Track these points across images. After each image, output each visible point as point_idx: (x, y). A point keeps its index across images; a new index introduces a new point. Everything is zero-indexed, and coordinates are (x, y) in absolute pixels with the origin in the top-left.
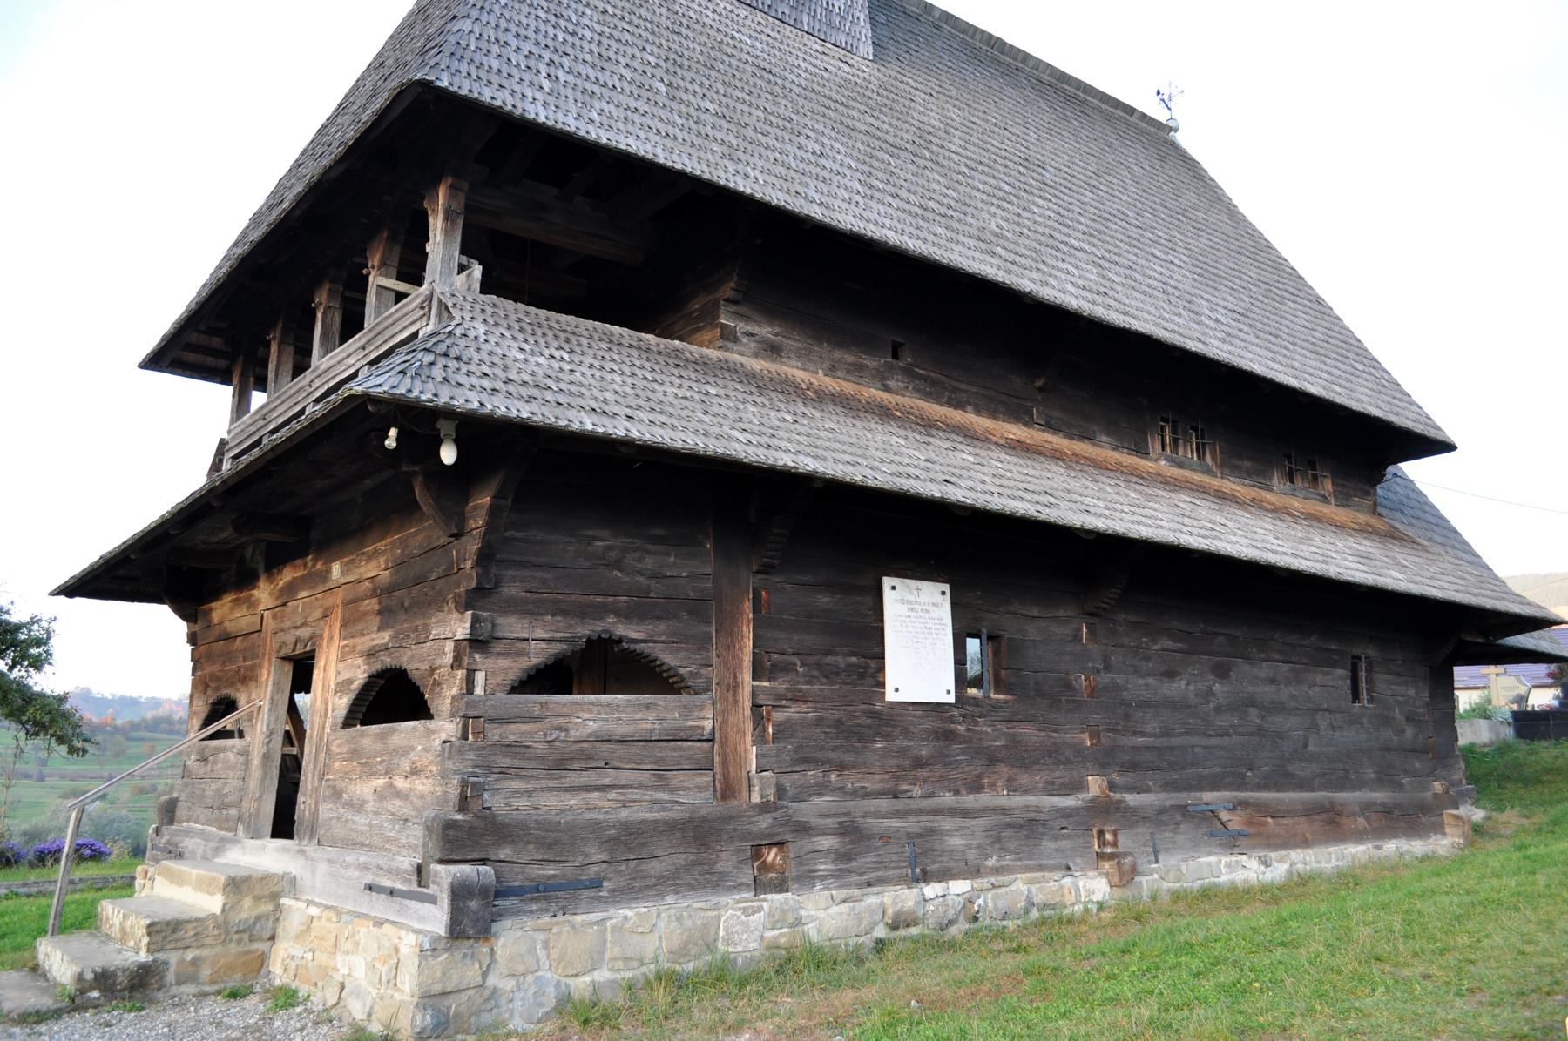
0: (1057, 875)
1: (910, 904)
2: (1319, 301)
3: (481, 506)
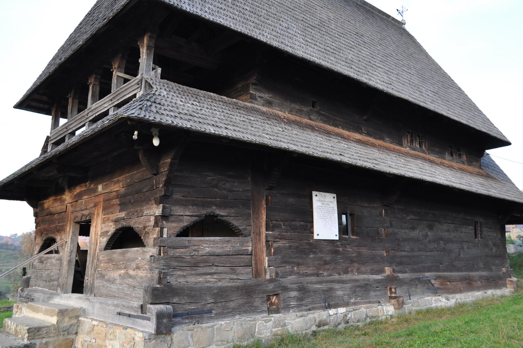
0: (376, 305)
1: (325, 317)
2: (460, 89)
3: (166, 163)
